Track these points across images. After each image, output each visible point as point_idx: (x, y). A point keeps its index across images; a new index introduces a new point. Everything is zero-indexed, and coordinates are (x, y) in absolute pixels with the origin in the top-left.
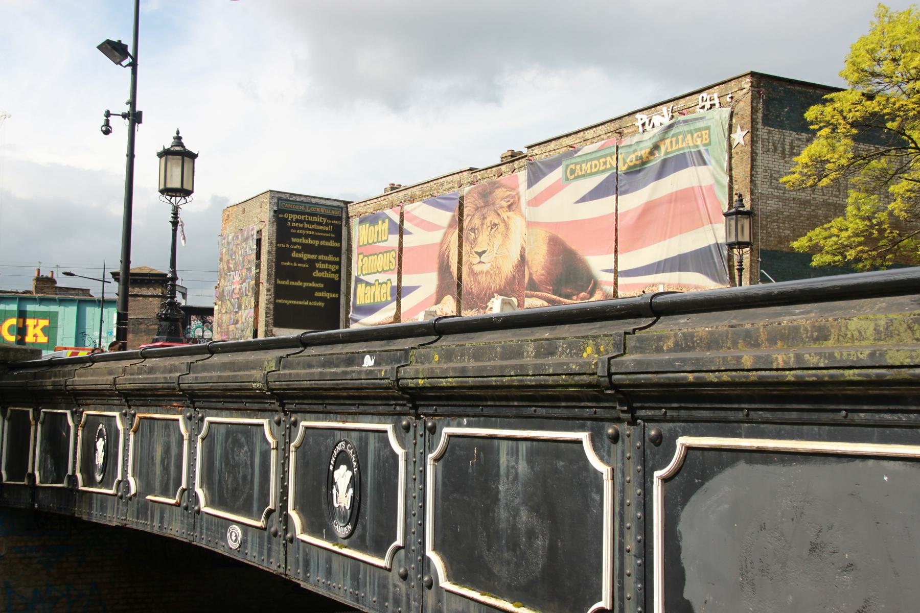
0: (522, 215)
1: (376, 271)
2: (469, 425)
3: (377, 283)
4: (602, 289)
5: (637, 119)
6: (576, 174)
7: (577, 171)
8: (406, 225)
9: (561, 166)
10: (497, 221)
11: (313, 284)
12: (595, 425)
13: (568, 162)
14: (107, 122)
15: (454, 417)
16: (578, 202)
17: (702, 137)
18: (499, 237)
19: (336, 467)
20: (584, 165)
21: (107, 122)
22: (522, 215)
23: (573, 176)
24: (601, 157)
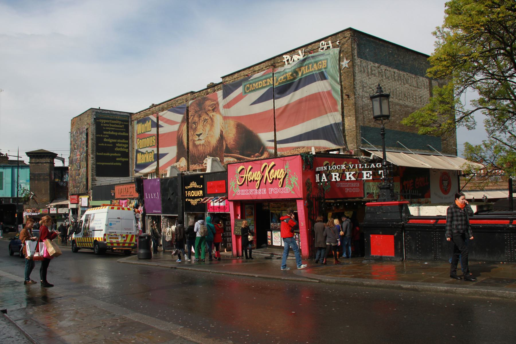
0: (220, 114)
3: (147, 152)
4: (267, 151)
6: (250, 90)
7: (250, 88)
8: (160, 123)
11: (115, 154)
13: (245, 83)
16: (252, 104)
20: (254, 85)
22: (220, 114)
23: (248, 91)
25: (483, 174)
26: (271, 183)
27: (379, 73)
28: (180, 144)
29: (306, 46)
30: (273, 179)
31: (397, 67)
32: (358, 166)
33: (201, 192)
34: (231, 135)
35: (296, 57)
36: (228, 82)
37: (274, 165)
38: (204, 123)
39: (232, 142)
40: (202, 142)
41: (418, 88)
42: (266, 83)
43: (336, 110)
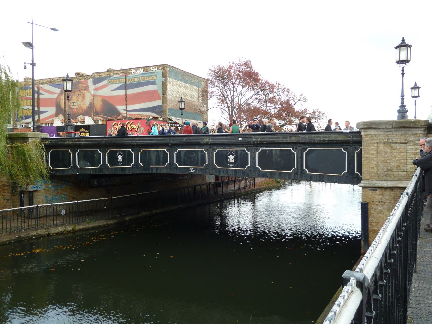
0: (90, 93)
1: (27, 105)
2: (266, 148)
3: (28, 109)
4: (122, 115)
5: (132, 71)
8: (40, 91)
9: (106, 80)
10: (80, 93)
12: (245, 147)
13: (109, 79)
14: (25, 65)
15: (217, 147)
16: (112, 91)
17: (154, 77)
18: (81, 98)
19: (118, 155)
20: (114, 81)
21: (25, 65)
22: (90, 93)
23: (110, 83)
24: (120, 79)
25: (38, 97)
26: (131, 130)
27: (177, 84)
28: (58, 106)
29: (144, 67)
30: (132, 128)
31: (185, 82)
32: (170, 125)
33: (88, 134)
34: (98, 104)
35: (138, 71)
36: (96, 76)
37: (133, 123)
38: (78, 96)
39: (99, 109)
40: (76, 107)
41: (193, 91)
42: (122, 81)
43: (160, 99)
